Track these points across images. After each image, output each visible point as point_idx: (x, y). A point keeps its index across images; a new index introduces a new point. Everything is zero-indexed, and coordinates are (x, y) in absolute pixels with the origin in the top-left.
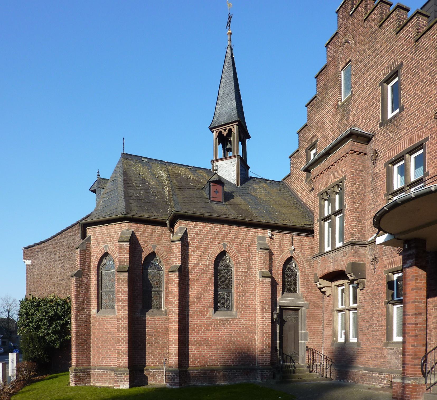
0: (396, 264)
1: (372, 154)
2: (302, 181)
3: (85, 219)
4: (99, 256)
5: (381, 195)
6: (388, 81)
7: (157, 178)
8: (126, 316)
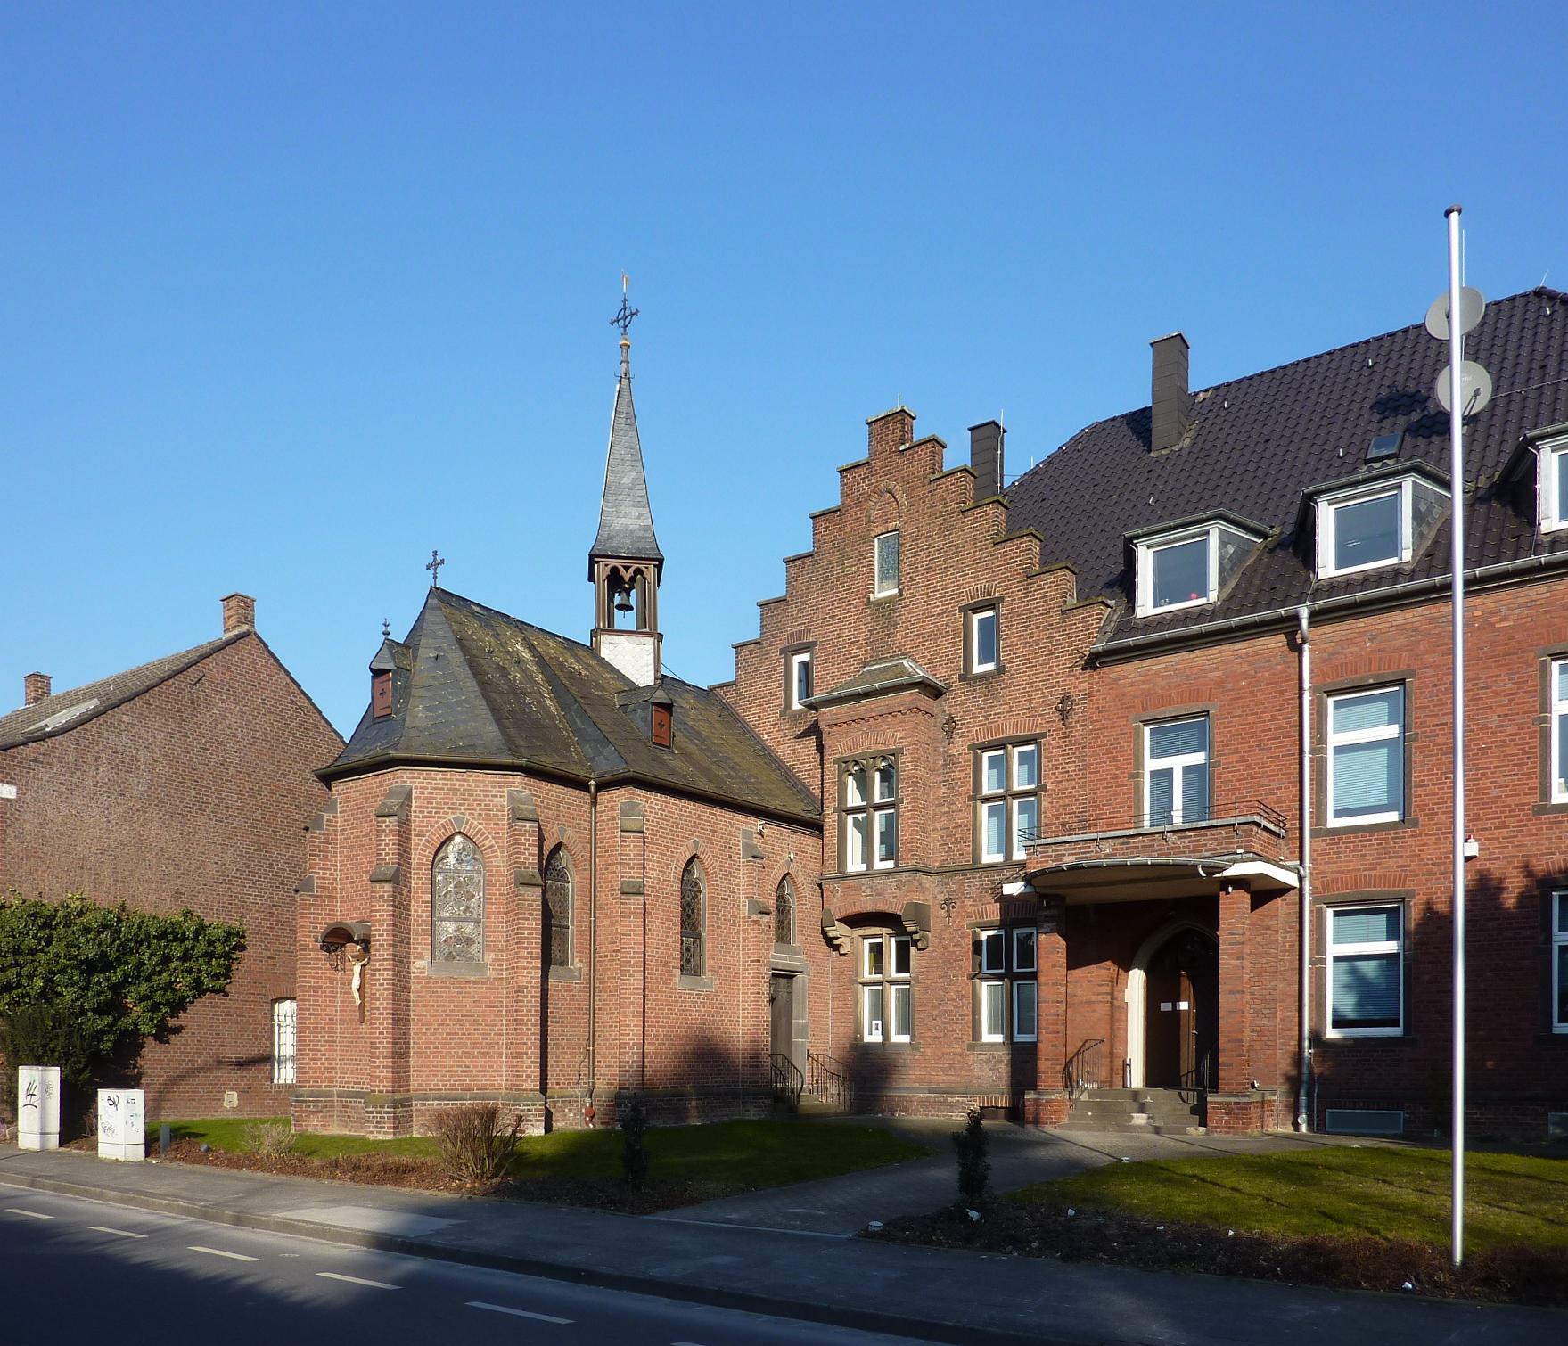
5: (961, 795)
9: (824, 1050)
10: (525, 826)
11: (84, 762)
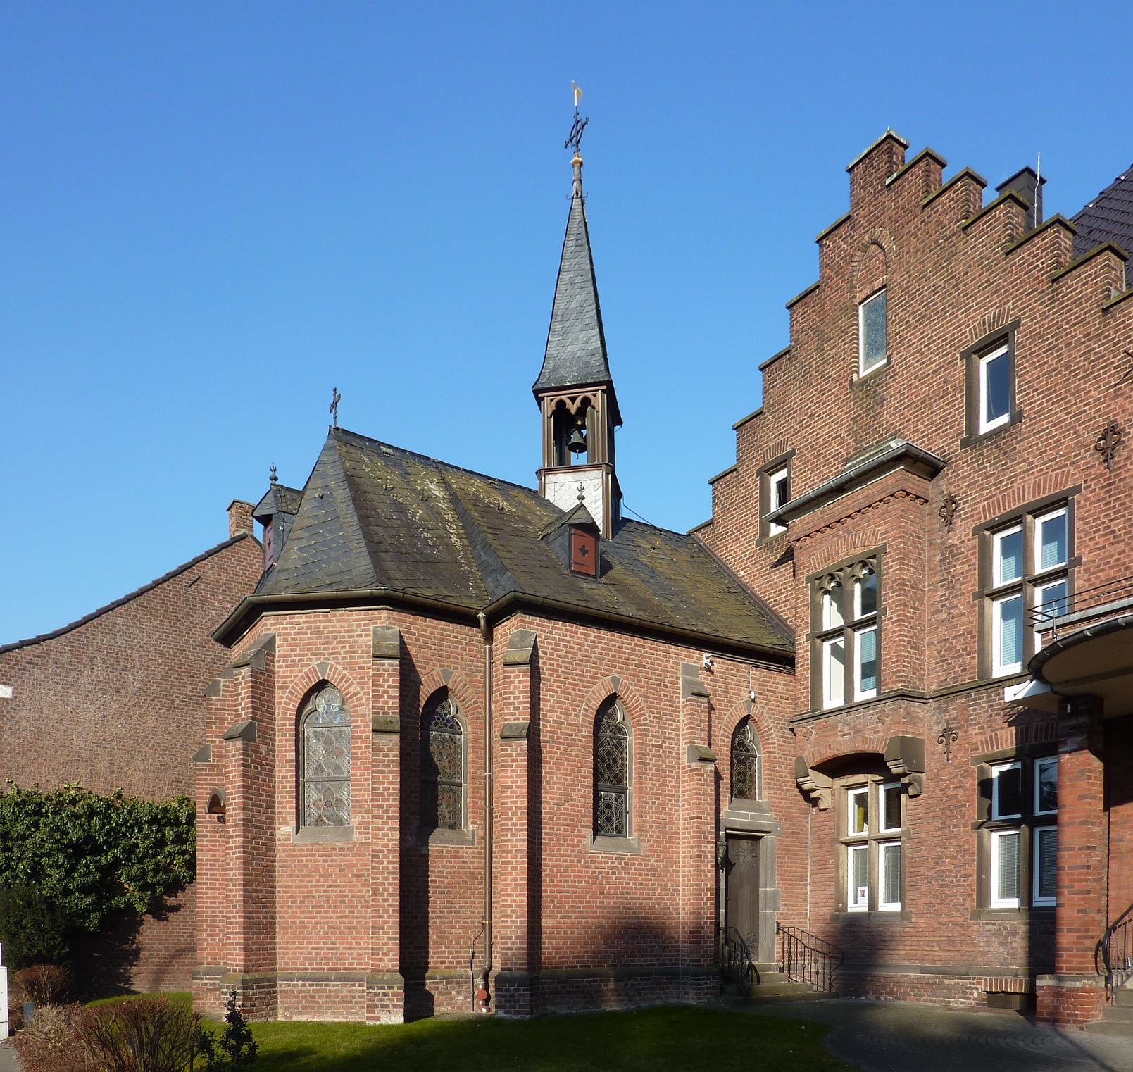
0: (1002, 745)
1: (942, 504)
2: (749, 542)
3: (161, 583)
4: (301, 689)
5: (964, 594)
6: (982, 350)
7: (427, 500)
8: (395, 845)
9: (801, 922)
10: (384, 665)
11: (79, 662)
